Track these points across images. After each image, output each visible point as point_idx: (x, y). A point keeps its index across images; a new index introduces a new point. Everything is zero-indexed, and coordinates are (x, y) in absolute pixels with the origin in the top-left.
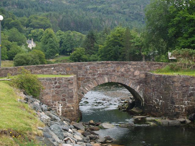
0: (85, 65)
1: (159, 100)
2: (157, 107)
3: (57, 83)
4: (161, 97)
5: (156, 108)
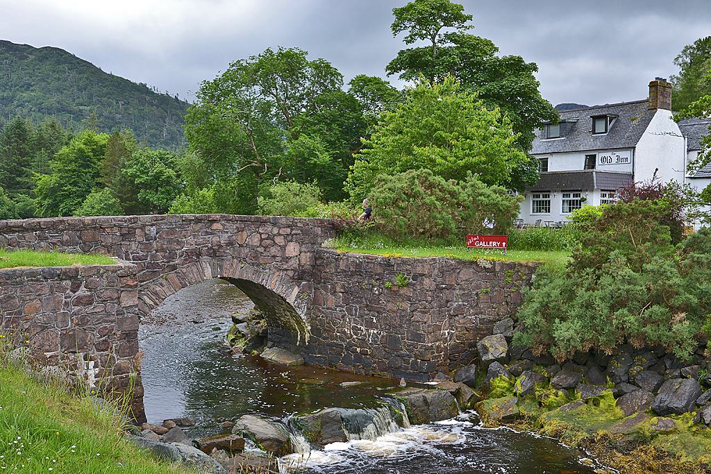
1: (367, 330)
2: (358, 350)
4: (375, 321)
5: (355, 351)
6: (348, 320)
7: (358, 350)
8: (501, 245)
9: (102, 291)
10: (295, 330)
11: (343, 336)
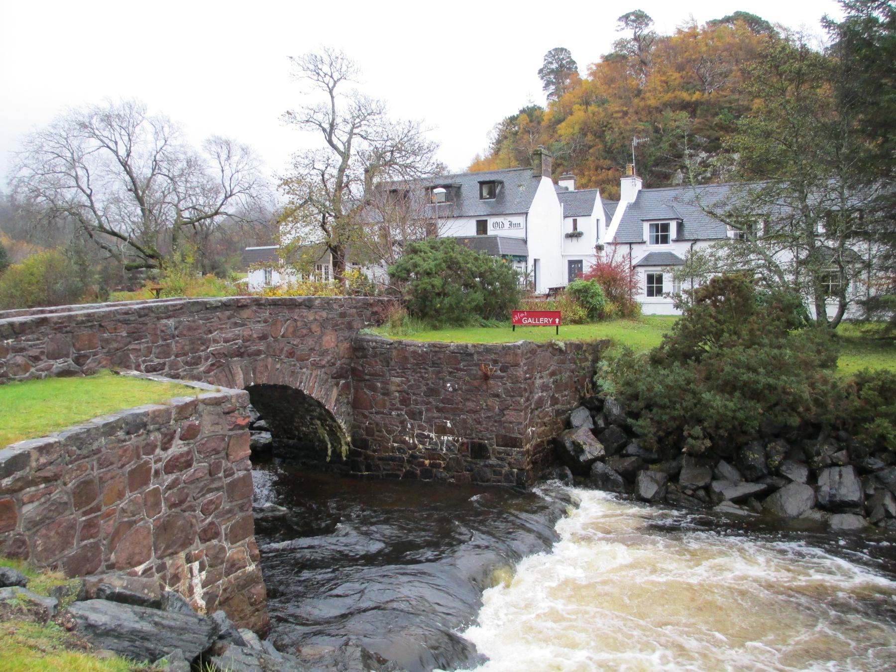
0: (159, 319)
1: (439, 437)
3: (177, 436)
4: (449, 425)
6: (409, 426)
7: (427, 462)
8: (554, 322)
9: (203, 442)
10: (323, 441)
11: (403, 446)
